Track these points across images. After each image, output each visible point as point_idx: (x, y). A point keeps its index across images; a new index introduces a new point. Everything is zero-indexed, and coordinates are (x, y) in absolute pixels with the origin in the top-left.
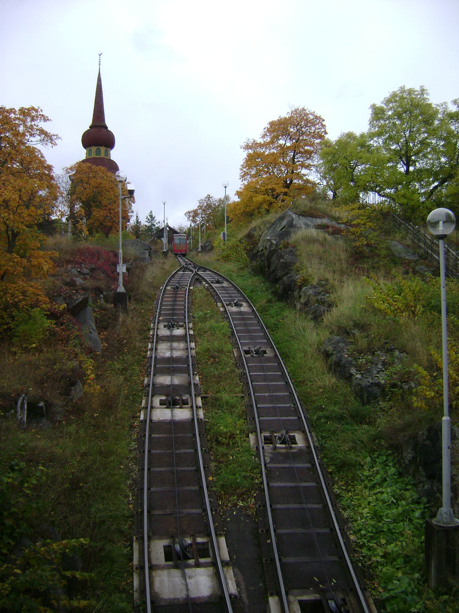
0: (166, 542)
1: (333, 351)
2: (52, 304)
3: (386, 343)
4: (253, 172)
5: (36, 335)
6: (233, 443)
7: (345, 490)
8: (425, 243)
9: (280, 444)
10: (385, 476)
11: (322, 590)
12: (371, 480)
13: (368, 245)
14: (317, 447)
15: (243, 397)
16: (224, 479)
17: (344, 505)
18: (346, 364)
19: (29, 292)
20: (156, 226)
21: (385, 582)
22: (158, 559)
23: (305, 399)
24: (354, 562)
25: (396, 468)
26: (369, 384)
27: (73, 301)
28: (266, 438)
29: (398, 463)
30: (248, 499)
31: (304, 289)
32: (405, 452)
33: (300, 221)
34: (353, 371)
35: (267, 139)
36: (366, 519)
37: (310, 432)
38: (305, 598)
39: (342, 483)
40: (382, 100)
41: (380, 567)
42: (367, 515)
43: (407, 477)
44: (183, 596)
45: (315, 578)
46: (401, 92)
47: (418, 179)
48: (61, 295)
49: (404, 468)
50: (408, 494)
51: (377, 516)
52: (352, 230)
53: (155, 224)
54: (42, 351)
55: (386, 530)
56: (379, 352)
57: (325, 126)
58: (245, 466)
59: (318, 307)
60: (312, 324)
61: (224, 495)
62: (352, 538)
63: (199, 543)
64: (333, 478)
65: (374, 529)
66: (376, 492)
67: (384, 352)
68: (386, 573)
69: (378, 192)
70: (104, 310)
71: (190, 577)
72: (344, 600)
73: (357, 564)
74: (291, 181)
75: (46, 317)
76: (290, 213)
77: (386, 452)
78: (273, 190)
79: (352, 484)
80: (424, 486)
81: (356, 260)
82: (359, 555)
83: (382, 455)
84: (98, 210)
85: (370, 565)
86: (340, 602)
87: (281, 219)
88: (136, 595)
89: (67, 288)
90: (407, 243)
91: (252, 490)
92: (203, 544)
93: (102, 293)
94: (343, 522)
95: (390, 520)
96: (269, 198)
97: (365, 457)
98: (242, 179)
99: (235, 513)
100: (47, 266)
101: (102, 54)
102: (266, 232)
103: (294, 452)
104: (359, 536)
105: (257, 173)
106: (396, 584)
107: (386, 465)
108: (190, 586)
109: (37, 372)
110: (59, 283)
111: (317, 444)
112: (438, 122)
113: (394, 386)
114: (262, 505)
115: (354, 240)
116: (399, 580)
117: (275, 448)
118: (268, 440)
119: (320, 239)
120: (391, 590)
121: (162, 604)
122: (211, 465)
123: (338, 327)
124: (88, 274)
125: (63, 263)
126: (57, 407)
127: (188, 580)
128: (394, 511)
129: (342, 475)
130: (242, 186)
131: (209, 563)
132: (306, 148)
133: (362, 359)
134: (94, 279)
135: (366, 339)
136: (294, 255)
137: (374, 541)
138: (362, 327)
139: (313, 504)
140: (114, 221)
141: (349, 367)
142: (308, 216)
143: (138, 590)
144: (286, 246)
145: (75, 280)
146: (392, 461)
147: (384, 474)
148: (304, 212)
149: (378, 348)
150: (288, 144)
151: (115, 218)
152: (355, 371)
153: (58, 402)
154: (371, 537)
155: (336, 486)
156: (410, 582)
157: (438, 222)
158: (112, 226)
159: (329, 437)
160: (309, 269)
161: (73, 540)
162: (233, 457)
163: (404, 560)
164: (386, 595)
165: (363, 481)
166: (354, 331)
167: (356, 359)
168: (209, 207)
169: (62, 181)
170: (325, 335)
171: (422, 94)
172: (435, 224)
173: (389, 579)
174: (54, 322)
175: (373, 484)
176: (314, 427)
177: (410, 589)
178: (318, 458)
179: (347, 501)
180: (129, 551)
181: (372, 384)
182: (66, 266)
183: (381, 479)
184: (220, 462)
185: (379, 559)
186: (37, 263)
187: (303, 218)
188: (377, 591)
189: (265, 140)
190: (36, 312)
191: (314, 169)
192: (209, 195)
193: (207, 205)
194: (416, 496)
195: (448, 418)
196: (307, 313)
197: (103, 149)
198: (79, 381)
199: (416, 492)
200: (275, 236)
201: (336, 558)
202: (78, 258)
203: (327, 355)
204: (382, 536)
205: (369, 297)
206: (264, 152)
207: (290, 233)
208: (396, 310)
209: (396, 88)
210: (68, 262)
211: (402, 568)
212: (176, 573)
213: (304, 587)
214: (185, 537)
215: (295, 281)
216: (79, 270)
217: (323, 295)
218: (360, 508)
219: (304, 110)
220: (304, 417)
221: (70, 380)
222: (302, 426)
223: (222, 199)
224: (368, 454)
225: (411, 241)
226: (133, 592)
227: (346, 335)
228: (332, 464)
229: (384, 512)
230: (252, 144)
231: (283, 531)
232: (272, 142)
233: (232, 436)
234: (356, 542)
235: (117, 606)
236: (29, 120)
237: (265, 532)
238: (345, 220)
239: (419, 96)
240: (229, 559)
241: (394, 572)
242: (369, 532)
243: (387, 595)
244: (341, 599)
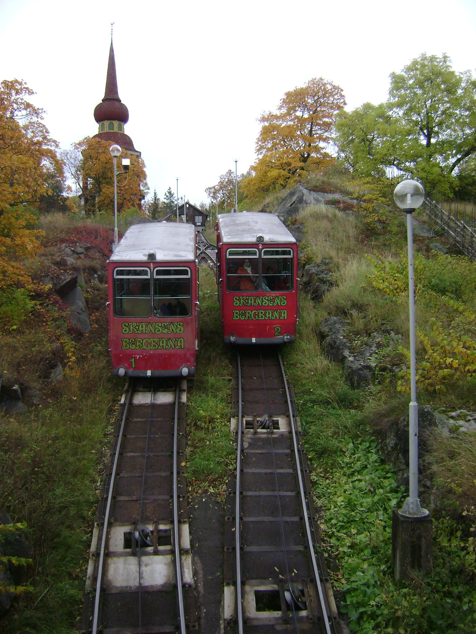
0: (127, 529)
1: (329, 332)
3: (383, 324)
4: (269, 146)
5: (18, 316)
6: (212, 428)
7: (323, 477)
8: (442, 219)
10: (366, 463)
11: (281, 580)
12: (351, 467)
13: (379, 221)
15: (230, 380)
16: (197, 465)
17: (319, 493)
18: (340, 345)
19: (9, 272)
20: (175, 203)
21: (349, 574)
22: (116, 546)
24: (319, 552)
25: (378, 455)
26: (360, 367)
27: (61, 281)
28: (248, 423)
29: (382, 449)
30: (219, 485)
31: (307, 267)
32: (388, 438)
33: (310, 197)
34: (346, 353)
37: (294, 416)
38: (262, 588)
39: (321, 470)
40: (403, 68)
42: (341, 504)
44: (136, 584)
45: (275, 568)
46: (422, 60)
47: (440, 151)
50: (386, 482)
51: (351, 505)
52: (364, 205)
53: (174, 201)
55: (357, 519)
56: (375, 334)
57: (344, 96)
58: (220, 452)
61: (196, 481)
63: (161, 530)
64: (312, 464)
66: (353, 480)
68: (351, 564)
69: (397, 166)
70: (97, 290)
71: (146, 565)
74: (309, 155)
75: (29, 298)
76: (301, 188)
78: (289, 164)
79: (331, 471)
80: (403, 474)
82: (327, 545)
83: (366, 442)
84: (108, 186)
85: (336, 555)
87: (292, 194)
88: (88, 582)
89: (55, 268)
90: (422, 220)
91: (225, 476)
92: (166, 531)
93: (96, 272)
94: (314, 510)
95: (364, 509)
98: (257, 153)
99: (204, 500)
100: (32, 246)
101: (114, 23)
102: (277, 208)
104: (330, 526)
105: (273, 146)
106: (359, 576)
107: (369, 452)
108: (145, 575)
109: (15, 355)
110: (47, 263)
111: (300, 429)
112: (462, 91)
113: (384, 369)
114: (232, 492)
116: (363, 572)
117: (256, 433)
120: (354, 581)
121: (114, 591)
122: (187, 450)
123: (337, 307)
124: (82, 253)
126: (34, 390)
127: (144, 568)
128: (369, 500)
129: (322, 462)
130: (257, 161)
131: (168, 550)
133: (357, 340)
135: (364, 320)
137: (345, 531)
138: (360, 307)
139: (287, 491)
140: (125, 199)
141: (342, 349)
142: (319, 191)
143: (91, 577)
145: (66, 260)
146: (375, 448)
148: (316, 187)
151: (126, 195)
152: (348, 353)
153: (35, 385)
155: (314, 473)
157: (406, 195)
158: (123, 203)
159: (314, 422)
160: (314, 247)
161: (10, 525)
162: (210, 442)
164: (346, 587)
165: (342, 468)
166: (351, 312)
167: (351, 341)
169: (71, 157)
171: (445, 62)
172: (403, 197)
173: (353, 570)
174: (38, 303)
176: (299, 412)
177: (372, 582)
178: (298, 444)
179: (323, 488)
180: (89, 537)
181: (364, 366)
182: (60, 245)
183: (362, 466)
184: (196, 447)
185: (345, 549)
186: (20, 242)
187: (314, 193)
188: (340, 582)
189: (282, 111)
190: (19, 293)
191: (331, 142)
192: (231, 171)
193: (228, 180)
194: (394, 485)
195: (416, 404)
197: (116, 123)
198: (59, 364)
200: (283, 213)
202: (73, 237)
204: (353, 525)
205: (369, 276)
206: (281, 124)
207: (298, 210)
208: (396, 289)
209: (417, 56)
210: (62, 241)
211: (368, 559)
212: (133, 560)
213: (262, 577)
214: (148, 524)
216: (73, 249)
217: (326, 274)
218: (336, 496)
219: (321, 79)
221: (50, 362)
223: (245, 174)
224: (351, 440)
225: (427, 217)
229: (359, 501)
230: (268, 116)
232: (289, 114)
233: (212, 420)
234: (325, 532)
236: (13, 92)
237: (231, 520)
238: (356, 195)
239: (441, 64)
242: (340, 521)
243: (349, 587)
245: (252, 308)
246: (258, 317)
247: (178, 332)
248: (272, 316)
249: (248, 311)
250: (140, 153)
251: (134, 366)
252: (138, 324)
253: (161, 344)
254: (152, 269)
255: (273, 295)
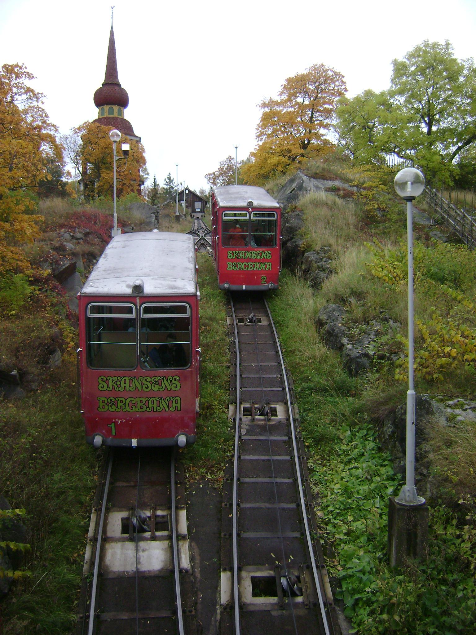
0: (124, 514)
2: (38, 269)
3: (381, 312)
5: (16, 301)
7: (320, 464)
9: (260, 415)
10: (363, 450)
11: (277, 567)
12: (348, 455)
14: (297, 420)
21: (345, 560)
22: (114, 531)
23: (293, 369)
25: (376, 443)
26: (358, 355)
27: (60, 267)
28: (246, 410)
30: (217, 472)
33: (310, 184)
34: (345, 340)
35: (284, 96)
36: (336, 494)
37: (291, 403)
38: (258, 574)
39: (318, 457)
40: (405, 54)
41: (342, 545)
42: (338, 491)
43: (386, 453)
45: (272, 554)
48: (47, 261)
49: (384, 442)
50: (383, 470)
51: (347, 492)
52: (364, 192)
53: (173, 186)
54: (22, 318)
55: (354, 507)
56: (374, 322)
57: (345, 83)
59: (319, 274)
60: (311, 291)
62: (319, 514)
63: (159, 516)
64: (309, 451)
65: (342, 506)
67: (380, 322)
68: (347, 551)
69: (398, 154)
71: (144, 550)
72: (298, 578)
73: (319, 541)
74: (309, 141)
76: (301, 175)
77: (367, 426)
78: (289, 151)
79: (328, 458)
80: (400, 462)
81: (367, 224)
82: (323, 532)
83: (363, 429)
84: (107, 172)
85: (333, 542)
86: (293, 578)
87: (292, 181)
88: (86, 567)
89: (54, 253)
90: (422, 208)
91: (222, 462)
92: (163, 517)
94: (311, 497)
95: (361, 497)
96: (285, 160)
97: (345, 431)
98: (258, 139)
99: (201, 486)
100: (31, 231)
103: (273, 425)
104: (326, 513)
105: (273, 133)
106: (355, 562)
107: (366, 440)
108: (142, 560)
110: (47, 248)
111: (297, 417)
112: (464, 79)
113: (382, 357)
114: (229, 479)
115: (365, 204)
116: (359, 559)
117: (253, 420)
118: (247, 411)
119: (329, 202)
120: (350, 568)
121: (111, 576)
124: (82, 238)
125: (56, 227)
127: (141, 554)
129: (319, 449)
130: (257, 147)
131: (165, 536)
132: (325, 106)
133: (356, 328)
134: (88, 243)
136: (300, 219)
137: (341, 518)
138: (359, 295)
140: (124, 184)
142: (319, 178)
143: (89, 561)
144: (293, 210)
145: (65, 245)
146: (373, 435)
147: (363, 448)
148: (316, 174)
149: (373, 317)
150: (307, 102)
152: (347, 341)
153: (34, 370)
154: (338, 513)
155: (311, 461)
156: (369, 561)
157: (406, 183)
158: (122, 189)
159: (311, 409)
160: (314, 234)
161: (8, 511)
163: (368, 538)
164: (342, 573)
165: (340, 455)
166: (350, 299)
167: (349, 329)
168: (230, 169)
169: (70, 142)
170: (321, 302)
171: (447, 48)
172: (403, 185)
173: (349, 557)
175: (349, 459)
176: (297, 399)
177: (368, 569)
178: (295, 431)
181: (362, 354)
182: (59, 230)
185: (342, 536)
186: (19, 227)
187: (314, 180)
188: (336, 569)
191: (332, 129)
192: (231, 157)
194: (391, 473)
195: (413, 392)
196: (306, 280)
197: (116, 108)
198: (58, 349)
199: (392, 469)
200: (282, 200)
201: (297, 535)
203: (320, 324)
205: (368, 264)
206: (281, 111)
208: (395, 278)
209: (419, 42)
210: (62, 226)
211: (364, 546)
212: (130, 546)
213: (259, 563)
215: (299, 247)
216: (72, 234)
219: (322, 65)
220: (289, 388)
221: (48, 347)
222: (286, 398)
223: (245, 161)
224: (348, 428)
225: (428, 205)
226: (84, 563)
227: (342, 303)
228: (310, 438)
230: (269, 102)
231: (248, 505)
232: (289, 100)
235: (64, 577)
237: (228, 506)
238: (356, 183)
239: (443, 51)
240: (186, 532)
241: (355, 550)
243: (344, 573)
244: (296, 576)
245: (243, 260)
246: (248, 268)
247: (173, 389)
248: (260, 267)
249: (239, 263)
250: (140, 138)
251: (114, 433)
252: (119, 378)
253: (150, 405)
254: (138, 305)
255: (261, 250)
